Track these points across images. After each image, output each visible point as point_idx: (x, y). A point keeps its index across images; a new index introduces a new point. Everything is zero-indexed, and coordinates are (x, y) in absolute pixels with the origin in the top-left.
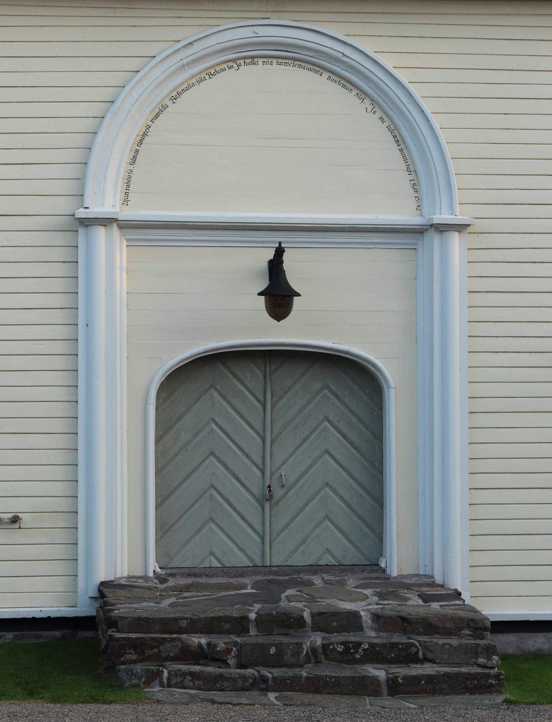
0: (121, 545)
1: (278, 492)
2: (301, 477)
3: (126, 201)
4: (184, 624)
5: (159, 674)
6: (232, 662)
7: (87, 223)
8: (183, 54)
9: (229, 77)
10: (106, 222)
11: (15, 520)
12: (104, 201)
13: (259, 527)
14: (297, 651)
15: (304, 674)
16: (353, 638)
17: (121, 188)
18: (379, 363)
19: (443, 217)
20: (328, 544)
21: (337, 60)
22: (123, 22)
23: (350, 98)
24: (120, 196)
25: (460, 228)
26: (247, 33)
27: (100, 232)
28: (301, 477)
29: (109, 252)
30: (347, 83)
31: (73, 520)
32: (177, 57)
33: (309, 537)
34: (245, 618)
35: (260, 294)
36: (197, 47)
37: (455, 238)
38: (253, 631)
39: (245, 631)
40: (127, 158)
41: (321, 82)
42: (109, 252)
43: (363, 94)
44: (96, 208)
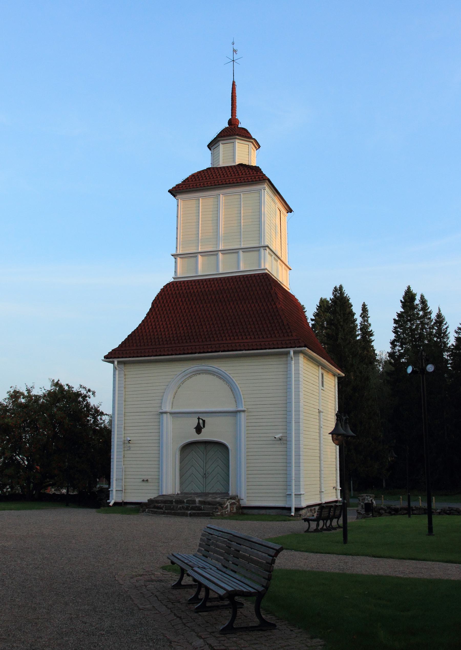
0: (170, 486)
1: (207, 475)
2: (213, 471)
3: (172, 408)
4: (160, 502)
5: (145, 510)
6: (164, 509)
7: (162, 413)
8: (183, 374)
9: (194, 378)
10: (166, 413)
11: (147, 480)
12: (168, 408)
13: (202, 483)
14: (177, 508)
15: (53, 490)
16: (194, 505)
17: (171, 404)
18: (187, 441)
19: (240, 409)
20: (218, 488)
21: (217, 373)
22: (148, 369)
23: (221, 381)
24: (171, 406)
25: (244, 411)
26: (197, 368)
27: (165, 415)
28: (213, 471)
29: (167, 419)
30: (220, 378)
31: (159, 480)
32: (181, 375)
33: (214, 487)
34: (172, 501)
35: (329, 434)
36: (186, 372)
37: (243, 414)
38: (174, 504)
39: (172, 503)
40: (172, 397)
41: (211, 377)
42: (167, 419)
43: (224, 380)
44: (164, 410)
